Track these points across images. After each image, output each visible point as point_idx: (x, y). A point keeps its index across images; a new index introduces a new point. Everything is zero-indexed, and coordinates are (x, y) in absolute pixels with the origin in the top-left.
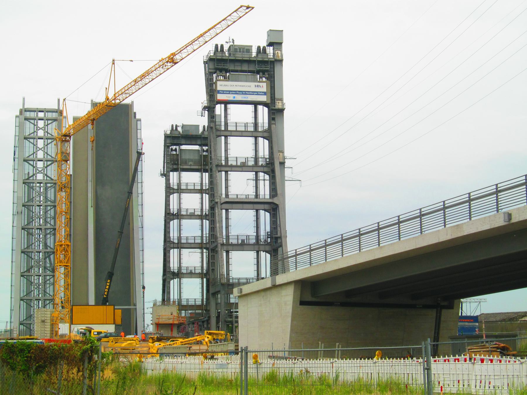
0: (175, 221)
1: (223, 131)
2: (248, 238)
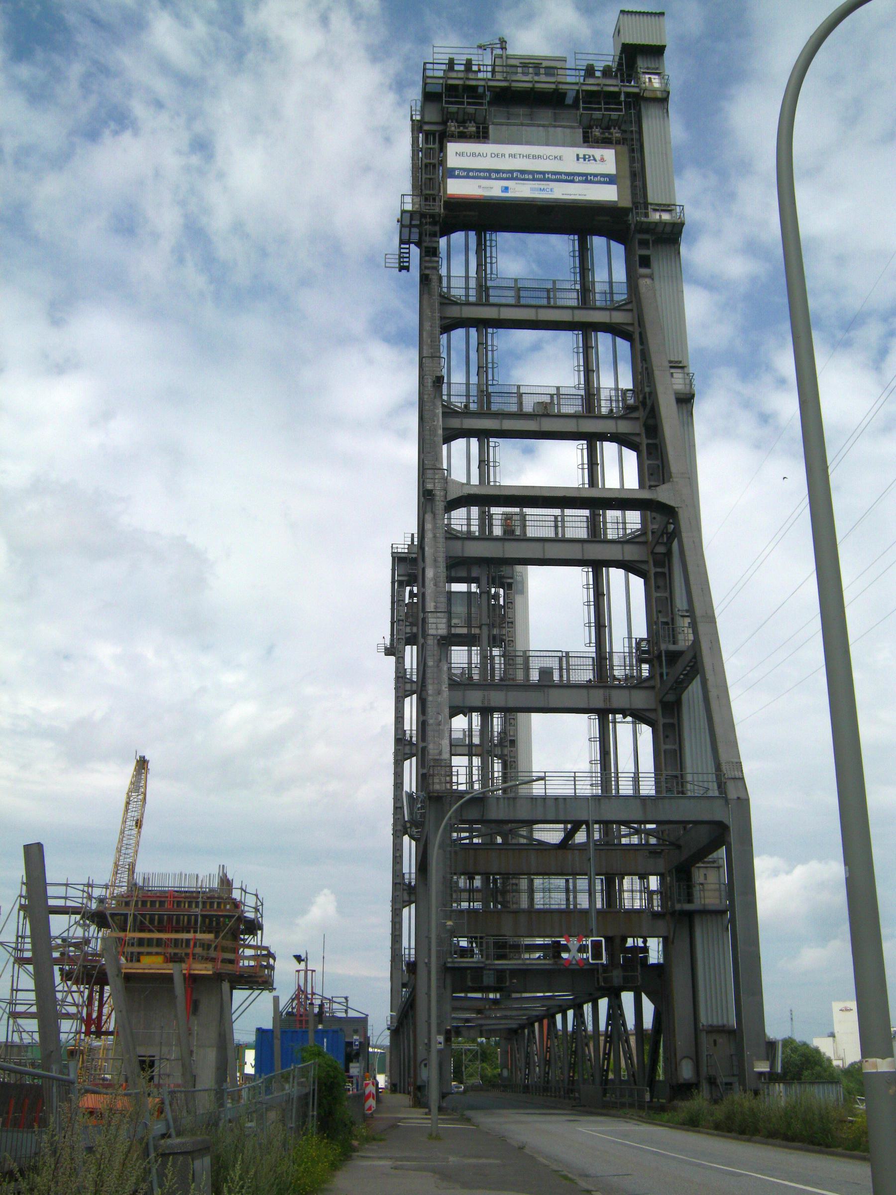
2: (564, 666)
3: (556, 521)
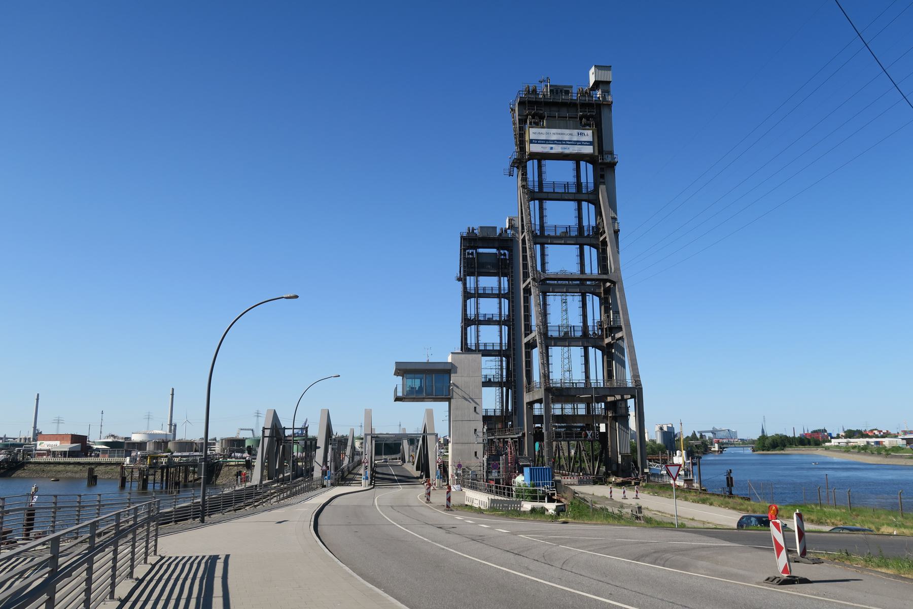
0: (473, 327)
3: (565, 186)
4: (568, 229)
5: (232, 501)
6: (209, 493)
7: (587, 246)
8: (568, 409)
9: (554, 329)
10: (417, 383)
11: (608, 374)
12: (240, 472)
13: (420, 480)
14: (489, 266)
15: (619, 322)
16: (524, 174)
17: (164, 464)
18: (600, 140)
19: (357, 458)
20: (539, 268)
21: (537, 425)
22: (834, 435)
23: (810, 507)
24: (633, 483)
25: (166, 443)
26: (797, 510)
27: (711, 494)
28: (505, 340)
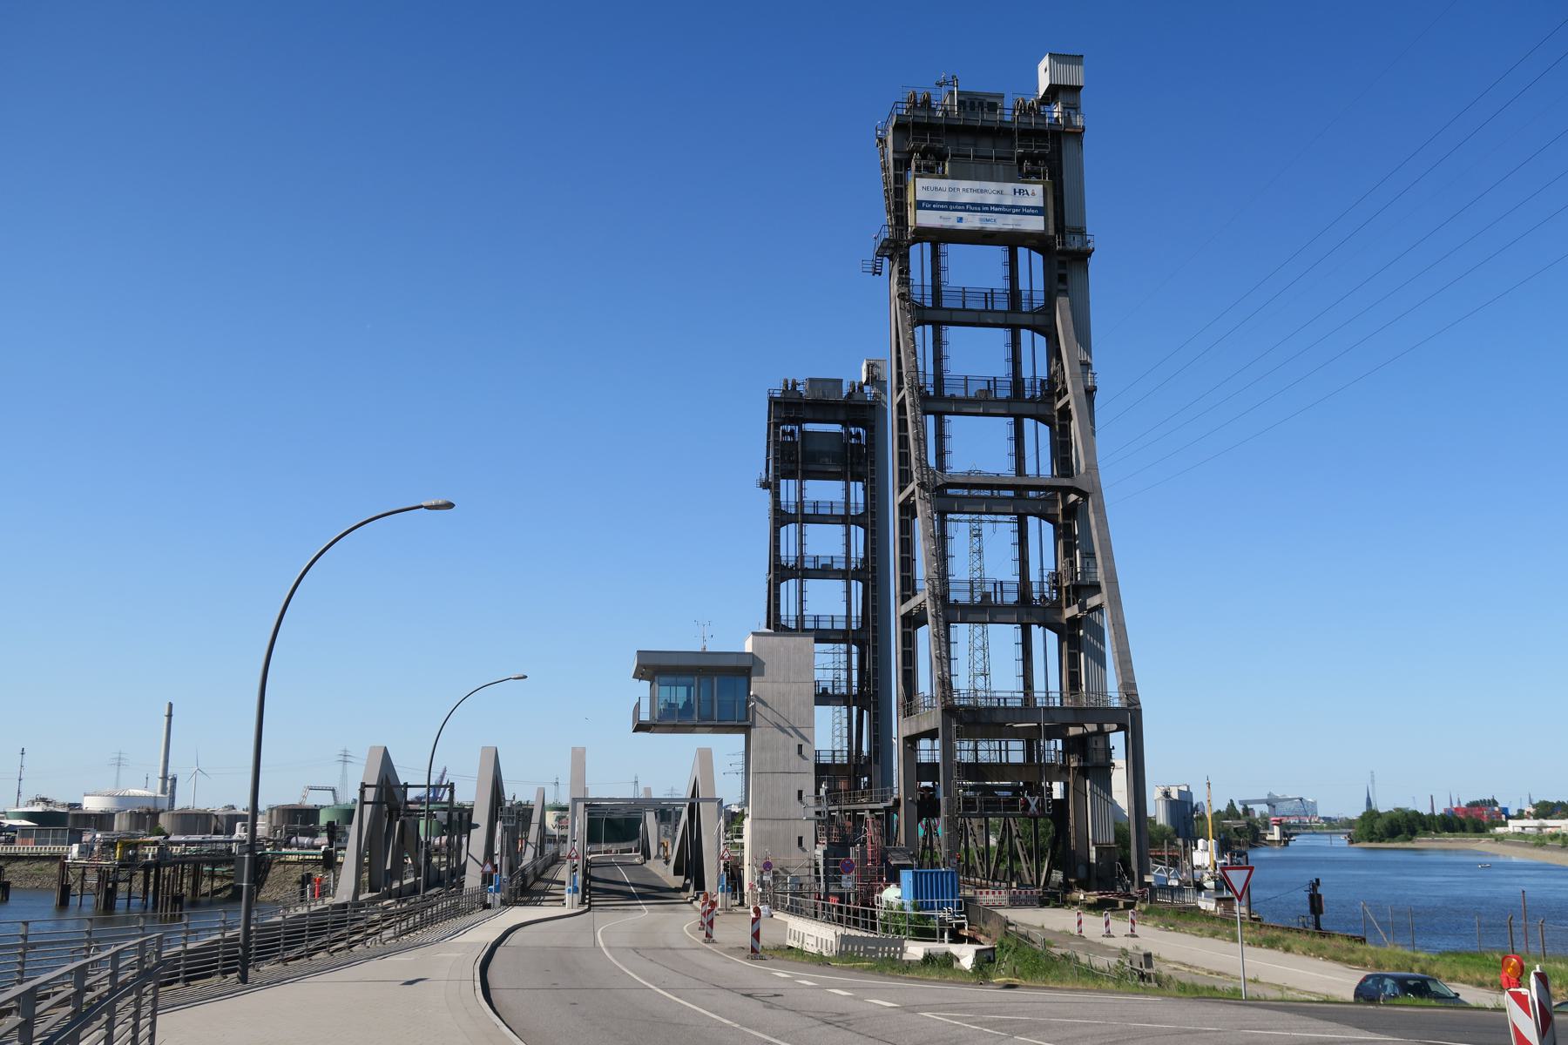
1: (929, 308)
3: (986, 297)
4: (992, 383)
5: (304, 931)
6: (256, 919)
7: (1029, 419)
8: (987, 752)
9: (960, 586)
10: (680, 695)
11: (1070, 681)
12: (309, 875)
13: (683, 894)
14: (827, 460)
15: (1093, 575)
16: (904, 272)
17: (150, 858)
18: (1059, 205)
19: (550, 849)
20: (932, 462)
21: (924, 784)
22: (1513, 812)
23: (1491, 958)
24: (1121, 905)
25: (155, 815)
26: (1538, 967)
27: (1283, 928)
28: (857, 610)
